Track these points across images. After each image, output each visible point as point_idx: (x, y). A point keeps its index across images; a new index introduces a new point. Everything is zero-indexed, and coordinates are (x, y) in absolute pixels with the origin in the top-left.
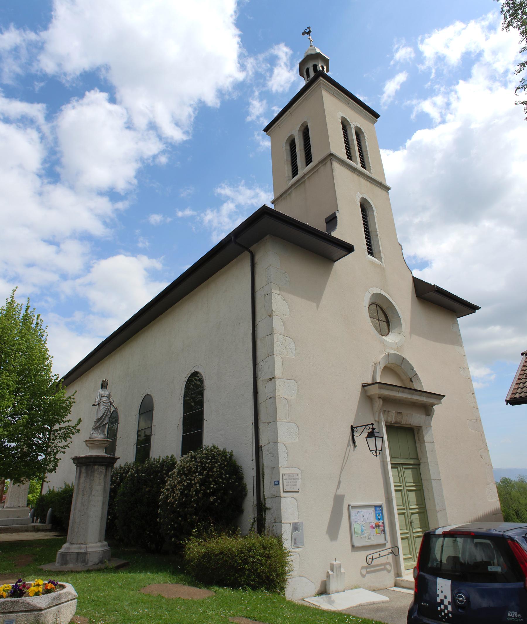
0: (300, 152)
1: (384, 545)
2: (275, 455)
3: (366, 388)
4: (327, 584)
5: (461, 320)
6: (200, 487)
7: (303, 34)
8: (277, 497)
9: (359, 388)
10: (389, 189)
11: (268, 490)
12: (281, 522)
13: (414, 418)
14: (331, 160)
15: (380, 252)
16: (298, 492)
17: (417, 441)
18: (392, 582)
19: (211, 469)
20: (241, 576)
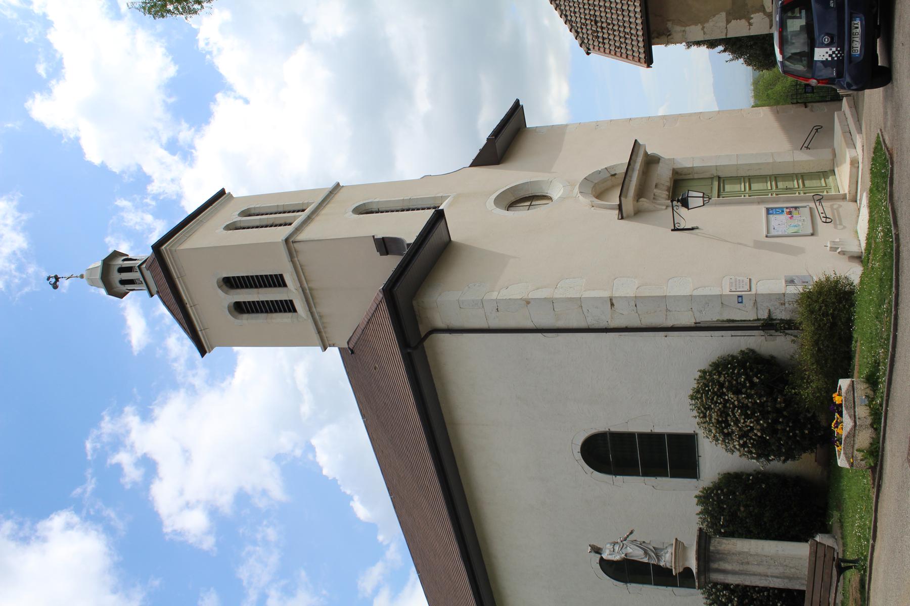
0: (260, 300)
2: (708, 300)
4: (851, 254)
6: (742, 393)
8: (756, 300)
9: (623, 222)
10: (338, 184)
11: (747, 314)
12: (784, 294)
13: (663, 174)
15: (435, 198)
17: (690, 177)
18: (852, 204)
19: (721, 385)
20: (840, 320)
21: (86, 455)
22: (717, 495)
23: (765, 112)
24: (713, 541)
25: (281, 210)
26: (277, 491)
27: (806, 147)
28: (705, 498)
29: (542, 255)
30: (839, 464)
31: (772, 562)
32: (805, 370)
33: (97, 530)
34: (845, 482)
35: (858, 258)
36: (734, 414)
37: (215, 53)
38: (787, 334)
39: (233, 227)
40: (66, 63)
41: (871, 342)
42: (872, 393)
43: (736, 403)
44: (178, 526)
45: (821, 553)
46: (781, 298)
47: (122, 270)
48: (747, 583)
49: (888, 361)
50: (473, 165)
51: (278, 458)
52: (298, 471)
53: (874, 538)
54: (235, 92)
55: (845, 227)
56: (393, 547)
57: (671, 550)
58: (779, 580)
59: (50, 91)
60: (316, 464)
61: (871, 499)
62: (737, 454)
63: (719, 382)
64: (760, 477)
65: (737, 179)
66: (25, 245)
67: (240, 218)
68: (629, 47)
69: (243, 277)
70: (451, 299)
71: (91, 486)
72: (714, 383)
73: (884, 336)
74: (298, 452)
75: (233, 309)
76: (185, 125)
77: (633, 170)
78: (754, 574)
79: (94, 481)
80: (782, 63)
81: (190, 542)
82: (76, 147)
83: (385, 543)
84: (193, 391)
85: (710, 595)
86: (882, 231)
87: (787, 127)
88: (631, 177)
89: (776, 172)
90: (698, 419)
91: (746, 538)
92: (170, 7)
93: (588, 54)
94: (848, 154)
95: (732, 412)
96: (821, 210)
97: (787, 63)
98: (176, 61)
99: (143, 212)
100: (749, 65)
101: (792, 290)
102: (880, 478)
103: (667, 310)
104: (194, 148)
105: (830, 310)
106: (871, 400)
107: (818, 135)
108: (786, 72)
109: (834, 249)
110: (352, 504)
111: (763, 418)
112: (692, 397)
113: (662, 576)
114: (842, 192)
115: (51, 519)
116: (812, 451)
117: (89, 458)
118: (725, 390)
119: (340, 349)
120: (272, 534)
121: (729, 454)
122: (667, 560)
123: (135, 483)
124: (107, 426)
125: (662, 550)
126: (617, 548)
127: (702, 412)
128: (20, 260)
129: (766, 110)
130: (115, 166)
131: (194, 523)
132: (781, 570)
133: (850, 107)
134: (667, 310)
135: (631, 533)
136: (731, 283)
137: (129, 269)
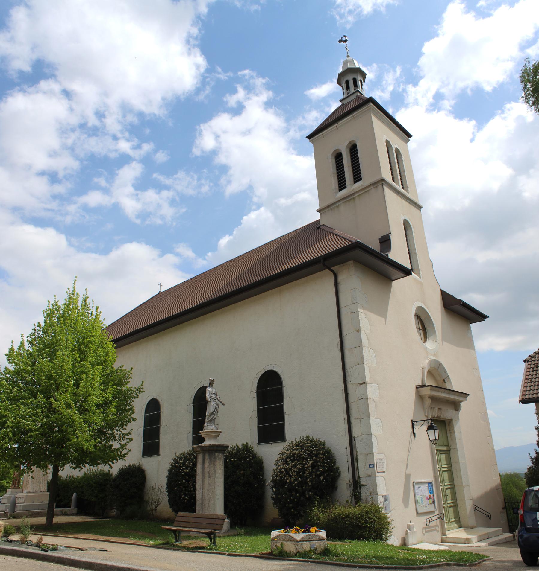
1: (434, 512)
2: (369, 445)
3: (419, 389)
5: (473, 326)
6: (312, 469)
7: (340, 41)
8: (372, 477)
10: (422, 208)
11: (362, 471)
12: (377, 494)
13: (448, 413)
14: (382, 185)
15: (418, 269)
16: (384, 472)
17: (448, 432)
18: (440, 541)
19: (316, 456)
20: (364, 532)
21: (241, 71)
22: (249, 456)
23: (497, 481)
24: (221, 455)
25: (402, 174)
26: (232, 189)
27: (476, 508)
28: (247, 449)
29: (391, 348)
30: (273, 532)
31: (211, 492)
32: (330, 509)
33: (197, 83)
34: (262, 537)
35: (404, 543)
36: (299, 464)
37: (503, 116)
38: (352, 497)
39: (388, 145)
40: (487, 20)
41: (351, 552)
42: (319, 552)
43: (306, 466)
44: (204, 132)
45: (218, 522)
46: (374, 493)
47: (355, 81)
48: (198, 477)
49: (339, 562)
50: (442, 292)
51: (251, 187)
52: (244, 201)
53: (230, 555)
54: (478, 132)
55: (424, 534)
56: (204, 262)
57: (214, 429)
58: (201, 496)
59: (467, 12)
60: (250, 211)
61: (253, 553)
62: (275, 468)
63: (319, 454)
64: (262, 483)
65: (449, 462)
66: (365, 13)
67: (394, 149)
68: (532, 388)
69: (358, 156)
70: (354, 282)
71: (223, 77)
72: (317, 451)
73: (355, 560)
74: (255, 199)
75: (338, 152)
76: (453, 102)
77: (449, 394)
78: (203, 481)
79: (226, 78)
80: (532, 490)
81: (196, 141)
82: (432, 35)
83: (206, 257)
84: (287, 130)
85: (190, 455)
86: (424, 559)
87: (488, 495)
88: (444, 392)
89: (456, 488)
90: (294, 441)
91: (224, 476)
92: (529, 85)
93: (525, 361)
94: (473, 537)
95: (301, 463)
96: (434, 518)
97: (533, 494)
98: (495, 89)
99: (395, 84)
100: (529, 469)
101: (380, 499)
102: (266, 558)
103: (361, 419)
104: (438, 112)
105: (369, 526)
106: (314, 551)
107: (484, 516)
108: (527, 493)
109: (409, 527)
110: (227, 235)
111: (298, 483)
112: (308, 437)
113: (198, 424)
114: (447, 532)
115: (201, 56)
116: (279, 516)
117: (239, 73)
118: (314, 458)
119: (319, 220)
120: (205, 189)
121: (274, 463)
122: (208, 427)
123: (227, 103)
124: (260, 82)
125: (214, 423)
126: (213, 396)
127: (299, 444)
128: (356, 11)
129: (498, 481)
130: (423, 61)
131: (208, 142)
132: (207, 498)
133: (506, 538)
134: (361, 419)
135: (223, 404)
136: (381, 460)
137: (356, 85)
